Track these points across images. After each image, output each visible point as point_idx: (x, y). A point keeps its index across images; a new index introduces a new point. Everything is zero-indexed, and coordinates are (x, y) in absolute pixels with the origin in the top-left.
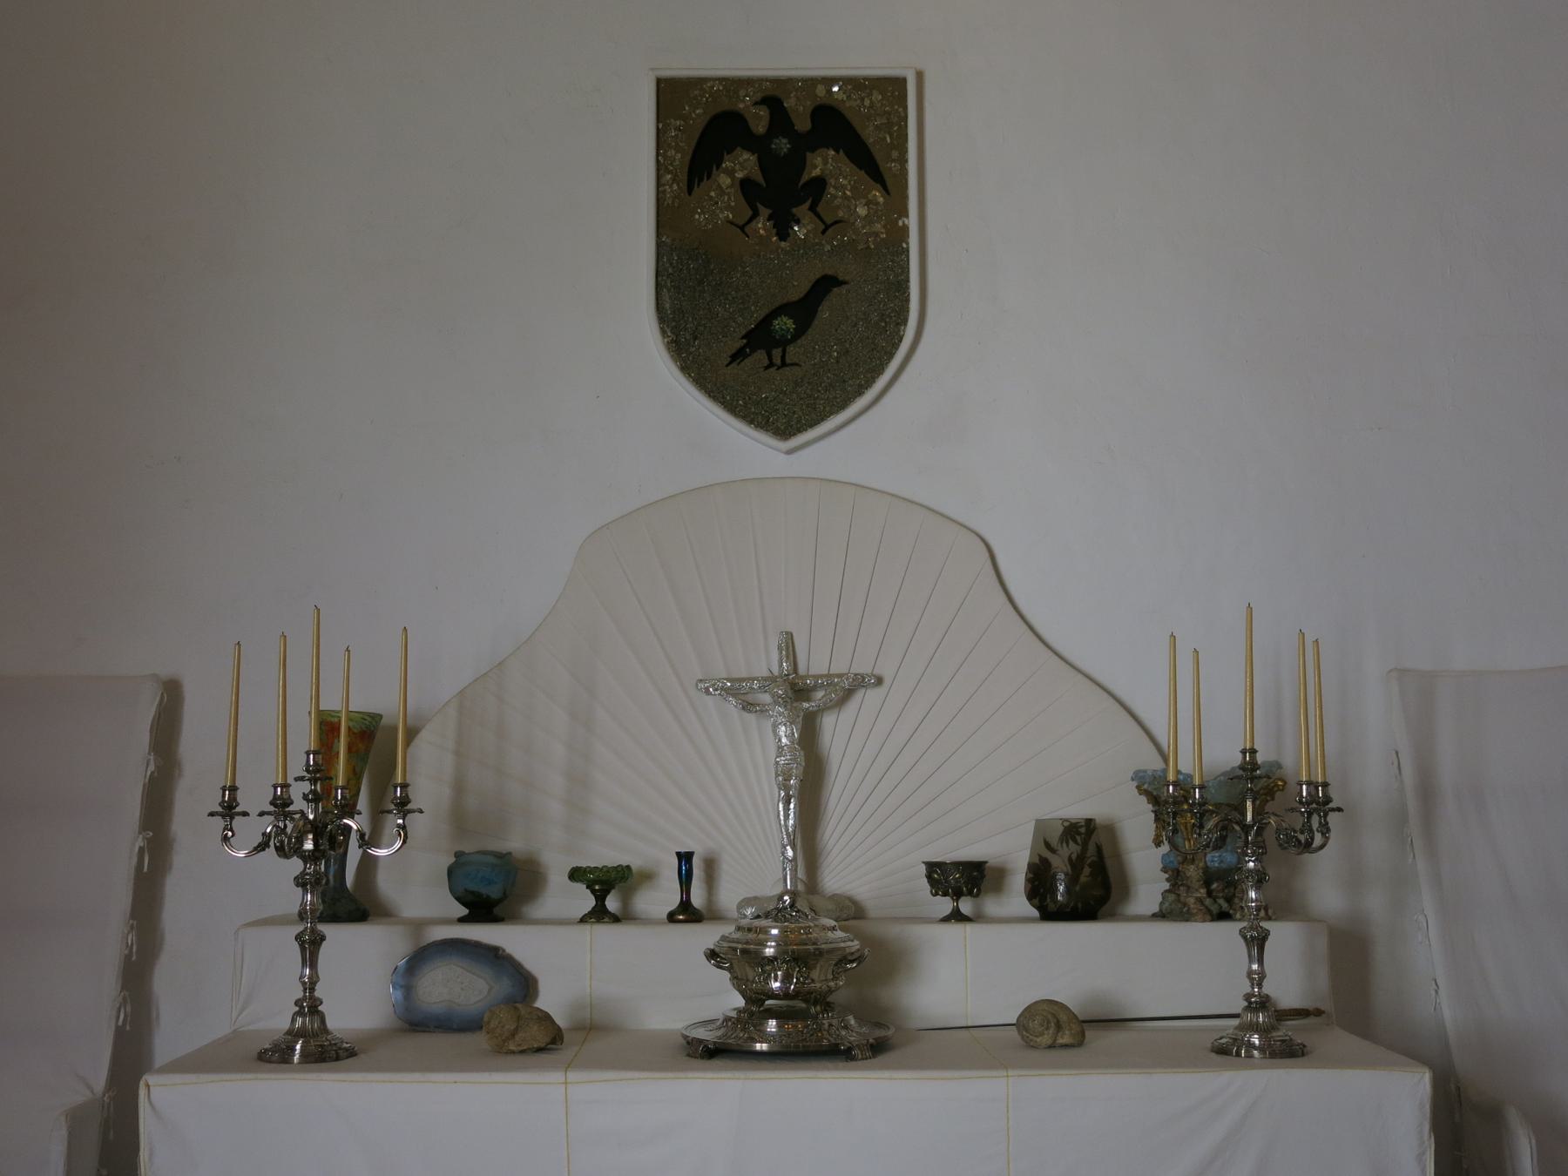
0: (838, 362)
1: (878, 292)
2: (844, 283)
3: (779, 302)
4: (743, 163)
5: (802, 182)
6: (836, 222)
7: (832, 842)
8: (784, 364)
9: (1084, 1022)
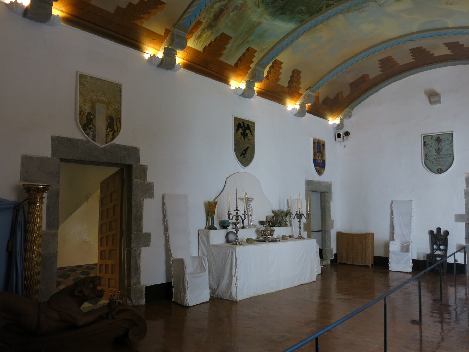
8: (245, 158)
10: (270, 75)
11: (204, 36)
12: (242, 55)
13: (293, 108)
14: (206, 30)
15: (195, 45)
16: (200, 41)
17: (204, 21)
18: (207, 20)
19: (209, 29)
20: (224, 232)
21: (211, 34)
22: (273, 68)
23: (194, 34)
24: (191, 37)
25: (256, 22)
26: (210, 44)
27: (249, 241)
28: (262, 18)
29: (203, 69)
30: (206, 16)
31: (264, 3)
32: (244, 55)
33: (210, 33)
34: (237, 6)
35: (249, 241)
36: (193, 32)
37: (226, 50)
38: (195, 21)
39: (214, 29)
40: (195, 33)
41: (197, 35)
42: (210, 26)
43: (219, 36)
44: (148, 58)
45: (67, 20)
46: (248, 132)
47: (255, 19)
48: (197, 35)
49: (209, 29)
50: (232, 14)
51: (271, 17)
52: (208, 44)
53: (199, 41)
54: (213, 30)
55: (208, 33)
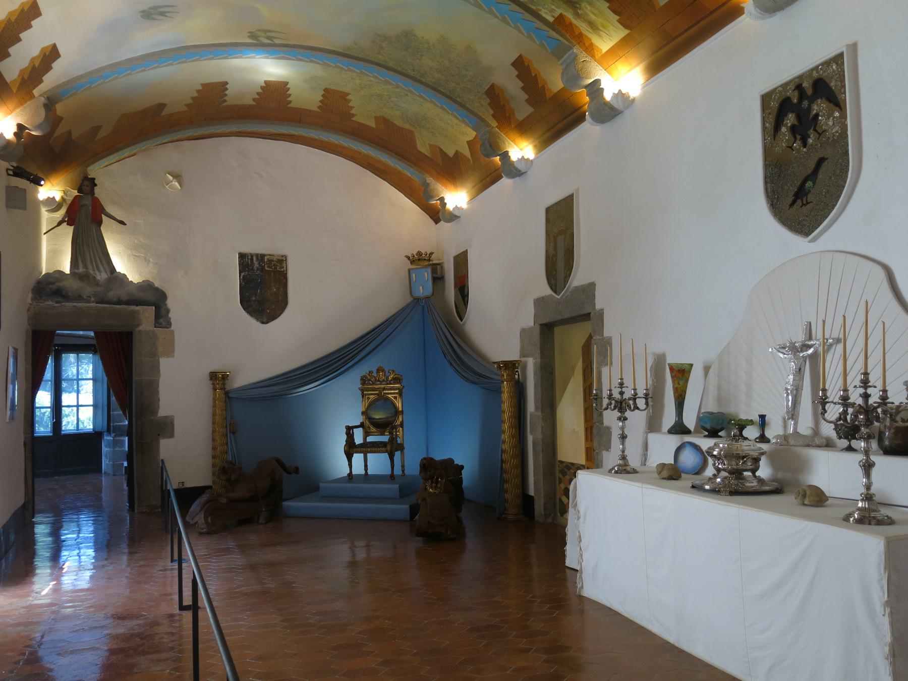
0: (825, 197)
1: (839, 159)
2: (827, 159)
3: (804, 176)
4: (790, 119)
5: (811, 116)
6: (823, 132)
7: (822, 426)
8: (807, 203)
9: (879, 503)
11: (593, 17)
14: (580, 12)
15: (611, 38)
16: (604, 28)
17: (559, 11)
18: (557, 7)
19: (578, 6)
20: (674, 441)
23: (584, 33)
24: (591, 40)
26: (615, 12)
27: (796, 425)
30: (546, 6)
33: (587, 6)
35: (796, 425)
36: (579, 34)
38: (548, 32)
40: (582, 31)
41: (587, 28)
45: (656, 66)
46: (820, 107)
48: (587, 28)
49: (578, 6)
52: (615, 16)
55: (586, 8)
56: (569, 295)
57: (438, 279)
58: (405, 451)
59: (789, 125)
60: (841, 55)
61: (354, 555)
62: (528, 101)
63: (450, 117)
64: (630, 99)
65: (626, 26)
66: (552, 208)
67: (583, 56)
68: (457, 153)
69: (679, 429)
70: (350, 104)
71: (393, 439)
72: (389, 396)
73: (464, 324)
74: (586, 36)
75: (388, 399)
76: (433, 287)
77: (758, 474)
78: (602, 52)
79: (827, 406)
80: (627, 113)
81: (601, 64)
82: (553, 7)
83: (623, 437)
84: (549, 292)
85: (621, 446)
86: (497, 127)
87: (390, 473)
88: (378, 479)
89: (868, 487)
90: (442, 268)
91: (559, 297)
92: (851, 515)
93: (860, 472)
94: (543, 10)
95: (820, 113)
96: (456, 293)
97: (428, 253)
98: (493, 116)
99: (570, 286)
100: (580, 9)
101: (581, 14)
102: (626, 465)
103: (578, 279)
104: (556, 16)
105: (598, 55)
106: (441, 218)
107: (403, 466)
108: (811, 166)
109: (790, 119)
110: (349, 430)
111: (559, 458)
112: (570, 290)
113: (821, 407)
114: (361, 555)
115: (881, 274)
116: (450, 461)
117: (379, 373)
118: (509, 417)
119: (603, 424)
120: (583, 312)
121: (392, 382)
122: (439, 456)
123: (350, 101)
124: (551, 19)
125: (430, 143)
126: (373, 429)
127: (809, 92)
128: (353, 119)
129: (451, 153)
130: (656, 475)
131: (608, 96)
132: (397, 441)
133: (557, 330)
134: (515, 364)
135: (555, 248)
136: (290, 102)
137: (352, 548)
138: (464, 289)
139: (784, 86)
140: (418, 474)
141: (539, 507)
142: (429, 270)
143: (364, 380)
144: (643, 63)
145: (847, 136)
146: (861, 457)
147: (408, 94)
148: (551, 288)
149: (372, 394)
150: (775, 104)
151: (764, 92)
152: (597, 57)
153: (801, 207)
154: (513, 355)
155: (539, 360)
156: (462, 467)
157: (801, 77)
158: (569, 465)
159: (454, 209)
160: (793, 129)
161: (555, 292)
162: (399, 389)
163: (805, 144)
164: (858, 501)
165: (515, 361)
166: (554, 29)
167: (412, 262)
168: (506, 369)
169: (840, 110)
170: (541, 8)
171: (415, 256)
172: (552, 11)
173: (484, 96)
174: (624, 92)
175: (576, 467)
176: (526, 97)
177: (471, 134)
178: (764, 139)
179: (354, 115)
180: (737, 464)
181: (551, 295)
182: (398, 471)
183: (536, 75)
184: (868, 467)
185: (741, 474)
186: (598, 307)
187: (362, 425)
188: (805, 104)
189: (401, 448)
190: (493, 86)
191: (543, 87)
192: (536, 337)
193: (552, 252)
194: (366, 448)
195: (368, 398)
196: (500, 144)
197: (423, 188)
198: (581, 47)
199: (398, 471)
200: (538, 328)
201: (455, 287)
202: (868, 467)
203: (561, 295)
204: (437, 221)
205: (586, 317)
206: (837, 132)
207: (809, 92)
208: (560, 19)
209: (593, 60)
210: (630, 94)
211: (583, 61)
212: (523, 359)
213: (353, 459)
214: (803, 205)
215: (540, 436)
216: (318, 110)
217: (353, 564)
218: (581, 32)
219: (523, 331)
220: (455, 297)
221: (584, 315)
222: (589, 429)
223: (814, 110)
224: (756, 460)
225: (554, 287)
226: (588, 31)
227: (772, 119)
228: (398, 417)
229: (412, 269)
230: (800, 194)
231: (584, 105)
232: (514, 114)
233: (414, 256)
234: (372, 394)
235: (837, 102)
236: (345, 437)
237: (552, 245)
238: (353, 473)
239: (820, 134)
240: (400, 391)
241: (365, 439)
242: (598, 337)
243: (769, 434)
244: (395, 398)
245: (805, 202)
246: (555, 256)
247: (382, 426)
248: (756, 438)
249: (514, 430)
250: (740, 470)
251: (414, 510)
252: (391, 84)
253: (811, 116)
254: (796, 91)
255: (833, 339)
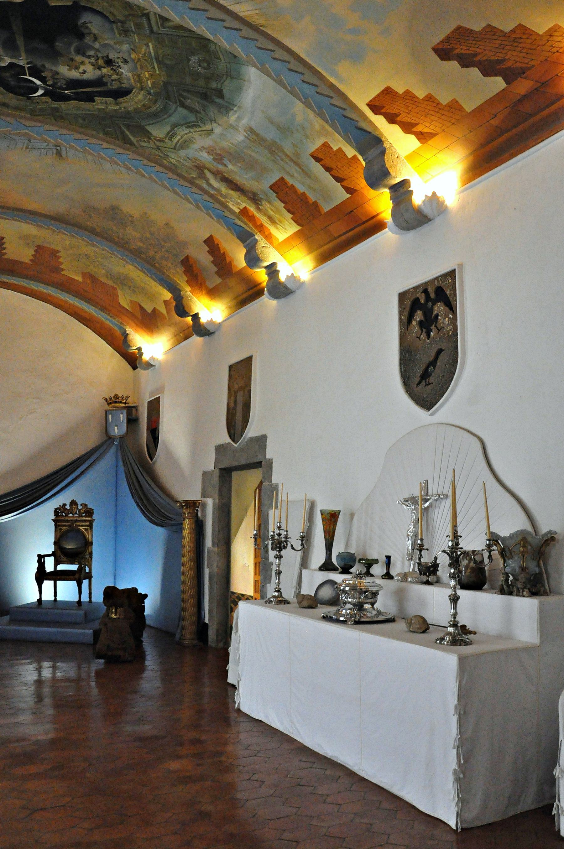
4: (419, 316)
5: (433, 315)
8: (430, 384)
10: (419, 128)
12: (328, 174)
13: (290, 275)
16: (281, 222)
17: (243, 205)
19: (259, 202)
21: (269, 202)
22: (397, 115)
24: (269, 230)
25: (246, 135)
28: (238, 126)
29: (358, 229)
31: (200, 124)
32: (328, 169)
34: (214, 159)
37: (307, 193)
39: (261, 196)
42: (255, 199)
43: (275, 195)
44: (444, 201)
46: (439, 308)
47: (240, 137)
49: (259, 202)
50: (230, 167)
51: (231, 113)
53: (278, 222)
54: (262, 199)
55: (266, 205)
56: (245, 444)
57: (132, 421)
58: (93, 580)
59: (418, 320)
60: (454, 271)
61: (40, 675)
62: (217, 273)
63: (150, 279)
64: (301, 281)
65: (298, 224)
66: (234, 366)
67: (262, 242)
68: (154, 310)
69: (327, 566)
70: (60, 260)
71: (80, 569)
72: (81, 528)
73: (154, 464)
74: (265, 227)
75: (79, 530)
76: (127, 427)
77: (376, 606)
78: (278, 241)
79: (423, 552)
80: (298, 293)
81: (277, 249)
82: (239, 201)
83: (279, 573)
84: (228, 440)
85: (452, 611)
86: (190, 291)
87: (77, 599)
88: (67, 604)
89: (455, 616)
90: (137, 410)
91: (236, 446)
92: (442, 639)
93: (448, 604)
94: (231, 202)
95: (440, 314)
96: (148, 435)
97: (125, 396)
98: (187, 281)
99: (246, 435)
100: (261, 205)
101: (262, 209)
102: (281, 595)
103: (251, 432)
104: (242, 208)
105: (275, 244)
106: (138, 366)
107: (90, 594)
108: (433, 353)
109: (419, 316)
110: (41, 558)
111: (232, 590)
112: (246, 440)
113: (418, 553)
114: (47, 673)
115: (478, 444)
116: (134, 590)
117: (72, 506)
118: (189, 552)
119: (268, 560)
120: (255, 461)
121: (83, 515)
122: (122, 586)
123: (59, 257)
124: (237, 211)
125: (131, 299)
126: (63, 558)
127: (433, 296)
128: (62, 273)
129: (149, 310)
130: (297, 605)
131: (282, 277)
132: (85, 570)
133: (235, 475)
134: (196, 503)
135: (235, 402)
136: (6, 254)
137: (39, 670)
138: (156, 431)
139: (416, 288)
140: (102, 600)
141: (212, 634)
142: (125, 412)
143: (56, 512)
144: (313, 253)
145: (457, 335)
146: (449, 592)
147: (113, 256)
148: (231, 438)
149: (65, 526)
150: (408, 303)
151: (401, 291)
152: (275, 245)
153: (425, 386)
154: (194, 495)
155: (217, 501)
156: (146, 596)
157: (426, 283)
158: (241, 596)
159: (150, 359)
160: (421, 324)
161: (233, 441)
162: (89, 521)
163: (428, 336)
164: (447, 627)
165: (196, 500)
166: (239, 219)
167: (109, 404)
168: (187, 508)
169: (452, 313)
170: (229, 201)
171: (113, 398)
172: (238, 204)
173: (179, 265)
174: (295, 275)
175: (236, 596)
176: (216, 269)
177: (168, 296)
178: (400, 329)
179: (62, 270)
180: (360, 598)
181: (229, 443)
182: (85, 598)
183: (224, 252)
184: (455, 599)
185: (362, 606)
186: (268, 457)
187: (53, 554)
188: (430, 304)
189: (89, 576)
190: (187, 258)
191: (230, 263)
192: (216, 479)
193: (232, 405)
194: (57, 576)
195: (61, 529)
196: (192, 307)
197: (123, 338)
198: (262, 235)
199: (85, 598)
200: (217, 473)
201: (147, 430)
202: (455, 599)
203: (238, 444)
204: (135, 368)
205: (258, 465)
206: (450, 330)
207: (433, 296)
208: (244, 212)
209: (271, 247)
210: (301, 277)
211: (263, 247)
212: (203, 499)
213: (44, 586)
214: (426, 385)
215: (215, 569)
216: (30, 262)
217: (39, 682)
218: (262, 223)
219: (205, 474)
220: (147, 438)
221: (257, 463)
222: (258, 564)
223: (435, 311)
224: (375, 594)
225: (232, 437)
226: (267, 223)
227: (406, 313)
228: (88, 548)
229: (109, 410)
230: (425, 375)
231: (263, 282)
232: (205, 282)
233: (111, 399)
234: (65, 526)
235: (451, 307)
236: (37, 565)
237: (233, 398)
238: (43, 599)
239: (439, 330)
240: (90, 524)
241: (55, 567)
242: (267, 483)
243: (393, 572)
244: (86, 530)
245: (427, 383)
246: (235, 408)
247: (70, 557)
248: (383, 576)
249: (192, 563)
250: (362, 602)
251: (96, 634)
252: (98, 247)
253: (433, 315)
254: (423, 294)
255: (443, 495)
